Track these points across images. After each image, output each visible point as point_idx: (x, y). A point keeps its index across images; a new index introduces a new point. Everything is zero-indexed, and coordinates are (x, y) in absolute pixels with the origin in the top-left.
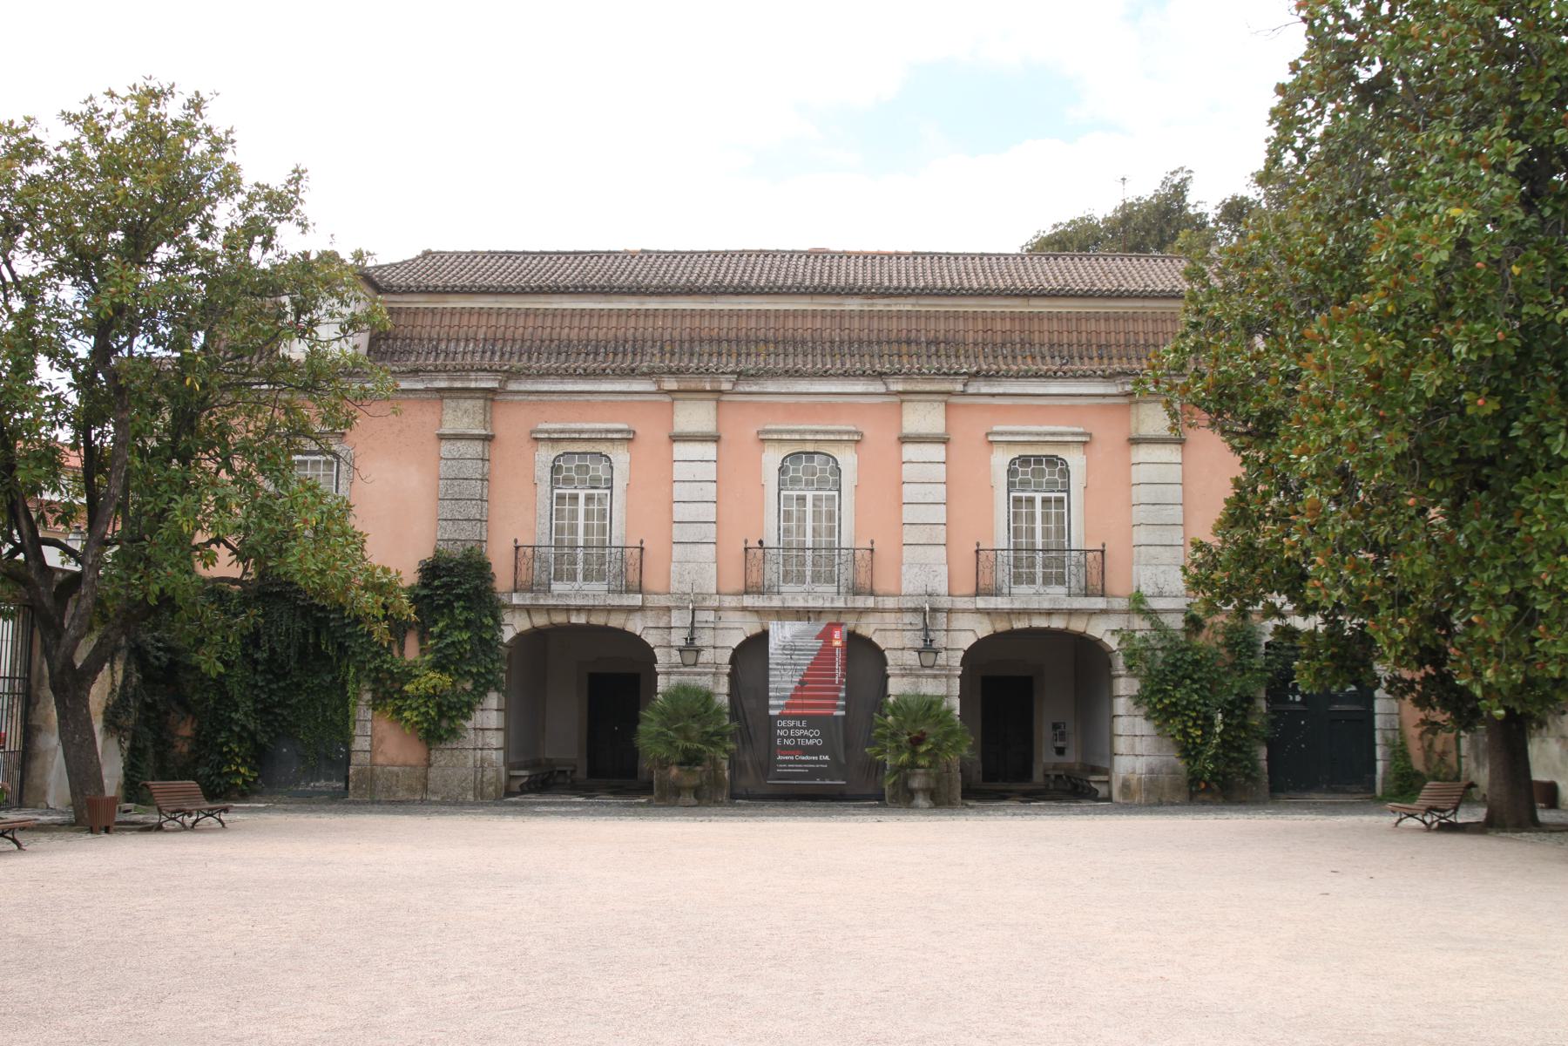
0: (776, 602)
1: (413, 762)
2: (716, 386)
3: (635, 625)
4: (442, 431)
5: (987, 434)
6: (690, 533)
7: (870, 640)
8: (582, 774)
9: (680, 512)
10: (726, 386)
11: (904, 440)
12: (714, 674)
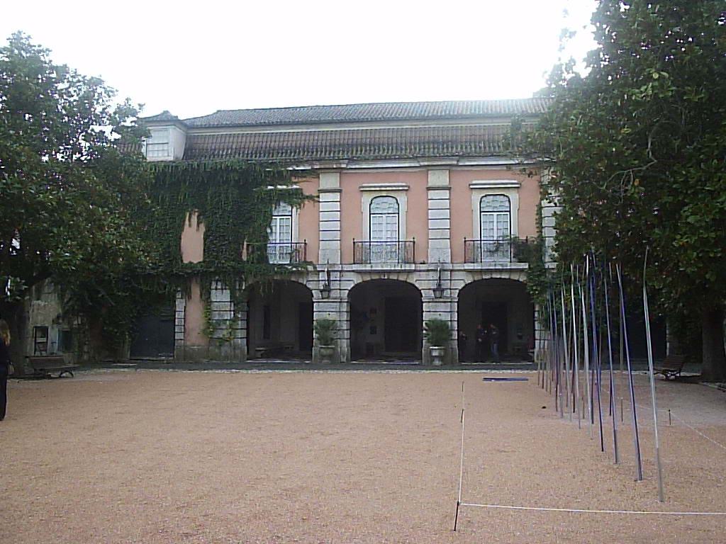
0: (368, 268)
1: (203, 344)
2: (339, 166)
3: (412, 279)
4: (320, 189)
5: (470, 185)
6: (328, 236)
7: (413, 285)
8: (297, 349)
9: (323, 226)
10: (344, 166)
11: (429, 189)
12: (340, 302)
